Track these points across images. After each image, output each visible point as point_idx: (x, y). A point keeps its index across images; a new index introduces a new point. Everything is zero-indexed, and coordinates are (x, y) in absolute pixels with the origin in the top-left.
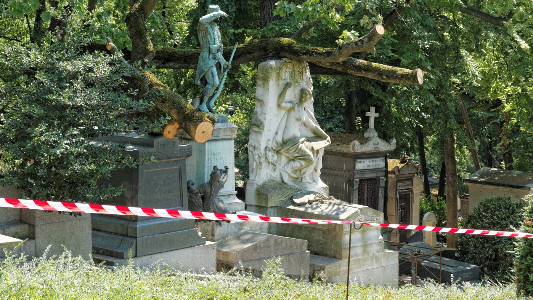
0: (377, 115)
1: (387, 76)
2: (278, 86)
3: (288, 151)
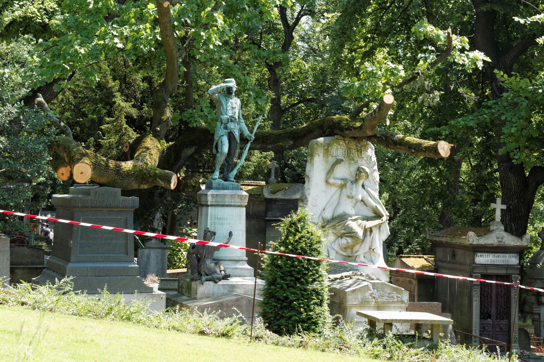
0: (504, 207)
1: (415, 149)
2: (327, 162)
3: (334, 227)
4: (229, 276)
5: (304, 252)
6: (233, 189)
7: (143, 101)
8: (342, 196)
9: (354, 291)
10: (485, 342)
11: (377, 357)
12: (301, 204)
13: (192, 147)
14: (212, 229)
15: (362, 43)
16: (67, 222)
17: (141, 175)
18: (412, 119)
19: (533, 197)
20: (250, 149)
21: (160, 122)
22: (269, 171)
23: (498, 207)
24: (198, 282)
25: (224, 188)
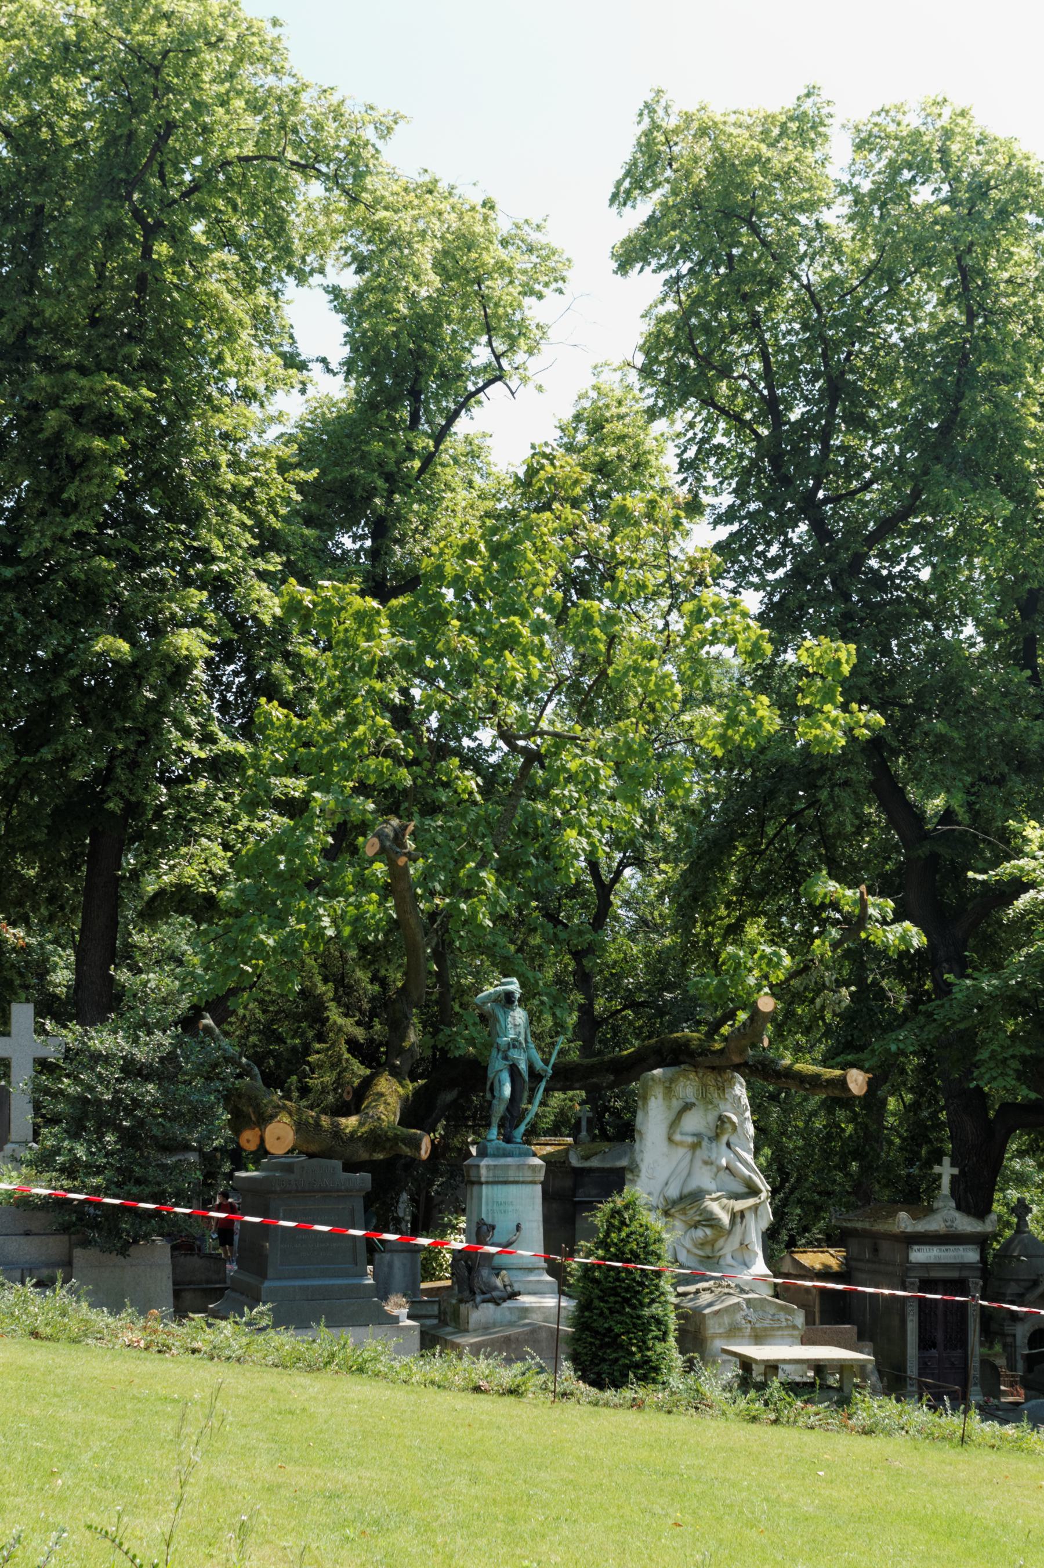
2: (669, 1108)
3: (683, 1212)
4: (519, 1294)
5: (636, 1257)
6: (520, 1155)
7: (373, 1014)
8: (697, 1161)
9: (717, 1312)
10: (928, 1386)
11: (754, 1419)
12: (629, 1176)
13: (453, 1089)
14: (489, 1221)
15: (723, 911)
16: (258, 1220)
17: (375, 1139)
18: (807, 1031)
19: (1003, 1149)
20: (546, 1090)
21: (400, 1052)
22: (579, 1121)
23: (946, 1171)
24: (469, 1305)
25: (505, 1155)
